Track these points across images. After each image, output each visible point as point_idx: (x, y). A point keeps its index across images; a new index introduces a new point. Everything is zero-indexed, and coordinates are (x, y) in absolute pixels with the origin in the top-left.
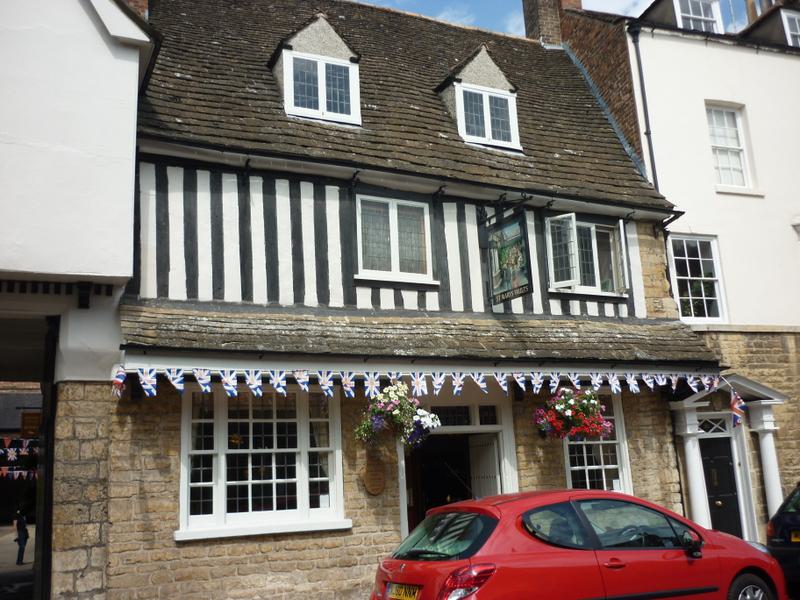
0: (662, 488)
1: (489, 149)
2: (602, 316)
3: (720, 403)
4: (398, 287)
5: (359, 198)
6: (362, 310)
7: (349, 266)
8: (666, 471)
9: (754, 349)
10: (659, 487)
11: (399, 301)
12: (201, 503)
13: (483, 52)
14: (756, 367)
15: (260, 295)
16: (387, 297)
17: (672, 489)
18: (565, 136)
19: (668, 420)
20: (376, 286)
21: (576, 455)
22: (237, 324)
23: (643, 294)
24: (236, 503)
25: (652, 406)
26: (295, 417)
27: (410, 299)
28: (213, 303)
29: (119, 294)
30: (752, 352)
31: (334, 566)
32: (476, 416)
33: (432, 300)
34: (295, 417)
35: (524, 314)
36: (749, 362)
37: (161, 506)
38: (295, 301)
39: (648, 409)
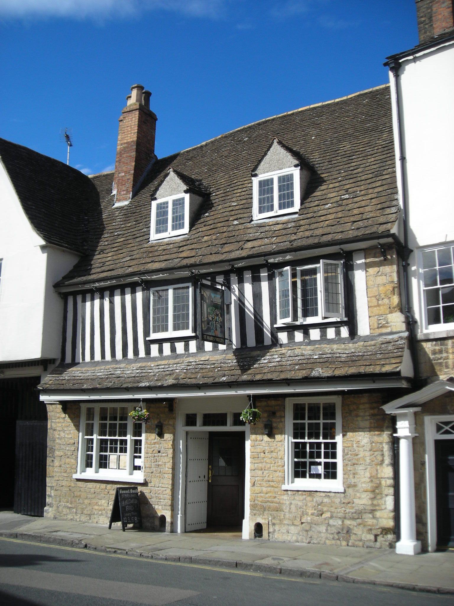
4: (172, 341)
6: (153, 358)
7: (146, 333)
10: (368, 480)
11: (173, 349)
18: (359, 179)
20: (160, 342)
21: (330, 450)
23: (367, 314)
25: (372, 411)
26: (127, 420)
27: (180, 347)
28: (185, 354)
32: (230, 420)
33: (345, 332)
34: (127, 420)
35: (288, 343)
37: (71, 462)
38: (123, 357)
39: (367, 414)
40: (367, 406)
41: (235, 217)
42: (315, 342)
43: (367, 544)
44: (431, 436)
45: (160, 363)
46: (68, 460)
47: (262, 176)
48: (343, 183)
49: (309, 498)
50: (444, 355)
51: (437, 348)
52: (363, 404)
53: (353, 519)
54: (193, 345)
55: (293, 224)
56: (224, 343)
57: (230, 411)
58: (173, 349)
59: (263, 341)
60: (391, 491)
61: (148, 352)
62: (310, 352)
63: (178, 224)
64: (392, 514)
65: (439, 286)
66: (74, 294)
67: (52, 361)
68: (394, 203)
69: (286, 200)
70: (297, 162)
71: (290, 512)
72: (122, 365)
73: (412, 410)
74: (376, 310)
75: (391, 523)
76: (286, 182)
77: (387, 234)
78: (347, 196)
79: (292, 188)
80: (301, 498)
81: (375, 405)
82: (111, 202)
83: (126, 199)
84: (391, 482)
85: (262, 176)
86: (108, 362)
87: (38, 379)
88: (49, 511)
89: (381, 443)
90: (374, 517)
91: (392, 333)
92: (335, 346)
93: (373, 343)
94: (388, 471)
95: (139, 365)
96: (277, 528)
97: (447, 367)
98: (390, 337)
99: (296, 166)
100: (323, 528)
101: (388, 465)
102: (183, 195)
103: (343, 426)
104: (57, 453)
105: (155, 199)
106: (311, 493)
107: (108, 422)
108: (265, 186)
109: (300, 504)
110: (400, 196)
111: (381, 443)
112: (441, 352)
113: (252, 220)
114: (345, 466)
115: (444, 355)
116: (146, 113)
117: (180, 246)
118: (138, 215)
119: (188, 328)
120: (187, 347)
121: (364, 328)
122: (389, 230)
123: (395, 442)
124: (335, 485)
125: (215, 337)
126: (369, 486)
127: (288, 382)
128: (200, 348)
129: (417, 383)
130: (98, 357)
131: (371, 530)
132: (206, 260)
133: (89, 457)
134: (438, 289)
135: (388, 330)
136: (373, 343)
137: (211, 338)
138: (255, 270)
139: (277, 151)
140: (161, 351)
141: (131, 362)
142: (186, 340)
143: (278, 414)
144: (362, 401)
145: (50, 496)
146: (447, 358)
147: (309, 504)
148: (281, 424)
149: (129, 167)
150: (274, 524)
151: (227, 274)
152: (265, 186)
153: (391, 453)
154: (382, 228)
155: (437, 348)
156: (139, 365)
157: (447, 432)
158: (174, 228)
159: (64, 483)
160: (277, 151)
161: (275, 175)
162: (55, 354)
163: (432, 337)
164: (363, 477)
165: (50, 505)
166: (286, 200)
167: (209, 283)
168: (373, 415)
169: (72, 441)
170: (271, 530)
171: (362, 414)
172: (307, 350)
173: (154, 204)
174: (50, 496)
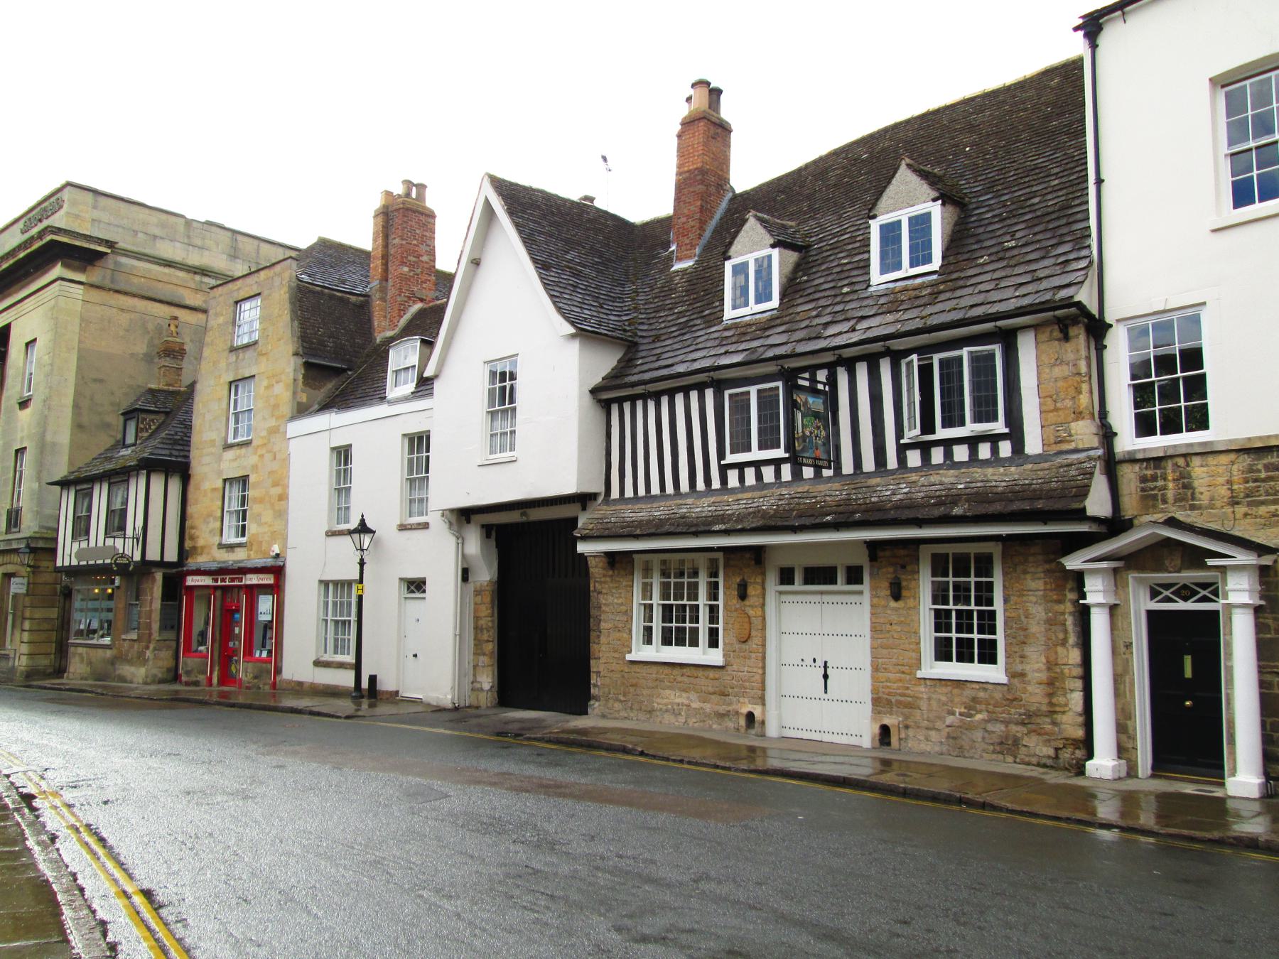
0: (1049, 669)
1: (899, 284)
2: (996, 459)
3: (1178, 562)
4: (757, 465)
5: (780, 384)
7: (721, 455)
8: (1060, 649)
9: (1263, 475)
11: (759, 476)
12: (648, 640)
13: (903, 167)
14: (1263, 503)
15: (670, 489)
16: (961, 453)
17: (1066, 671)
19: (1070, 585)
20: (741, 466)
22: (629, 514)
24: (666, 641)
25: (1047, 566)
29: (601, 499)
30: (1256, 480)
31: (714, 693)
32: (841, 577)
33: (1005, 449)
36: (1247, 496)
40: (1040, 557)
41: (846, 282)
42: (962, 464)
43: (1044, 761)
44: (1140, 604)
45: (740, 496)
46: (618, 635)
47: (884, 219)
48: (1009, 222)
49: (956, 691)
50: (1160, 483)
51: (1149, 472)
52: (1034, 554)
53: (1023, 724)
54: (786, 470)
55: (929, 290)
56: (829, 468)
57: (840, 562)
58: (759, 476)
59: (885, 464)
60: (1079, 684)
61: (724, 480)
62: (953, 480)
63: (763, 296)
64: (1081, 719)
65: (1153, 378)
66: (620, 401)
67: (593, 496)
68: (1084, 253)
69: (921, 253)
70: (936, 194)
71: (930, 710)
72: (690, 501)
73: (1104, 565)
74: (1052, 417)
75: (1080, 733)
76: (921, 224)
77: (1069, 303)
78: (1013, 243)
79: (910, 247)
80: (945, 690)
81: (1052, 557)
82: (669, 261)
83: (690, 257)
84: (1078, 671)
85: (884, 219)
86: (656, 496)
87: (574, 521)
88: (595, 706)
89: (1063, 614)
90: (1054, 723)
91: (1076, 451)
92: (990, 471)
93: (1046, 465)
94: (1075, 656)
95: (712, 499)
96: (911, 732)
97: (1165, 501)
98: (1075, 456)
99: (934, 200)
100: (978, 735)
101: (1073, 646)
102: (769, 251)
103: (1004, 586)
104: (603, 625)
105: (729, 258)
106: (960, 684)
107: (672, 580)
108: (891, 232)
109: (944, 698)
110: (1094, 242)
111: (1063, 614)
112: (1154, 478)
113: (869, 286)
114: (1008, 646)
115: (1160, 483)
116: (715, 124)
117: (765, 326)
118: (705, 287)
119: (778, 446)
120: (778, 474)
121: (1033, 445)
122: (1072, 297)
123: (1083, 614)
124: (994, 673)
125: (815, 459)
126: (1043, 676)
127: (919, 523)
128: (797, 474)
129: (1116, 525)
130: (655, 490)
131: (1049, 741)
132: (801, 348)
133: (648, 630)
134: (1153, 383)
135: (1072, 446)
136: (1046, 465)
137: (810, 461)
138: (873, 362)
139: (905, 179)
140: (742, 478)
141: (701, 495)
142: (777, 463)
143: (909, 568)
144: (1032, 551)
145: (595, 686)
146: (1165, 488)
147: (957, 700)
148: (913, 583)
149: (692, 208)
150: (907, 727)
151: (831, 367)
152: (891, 232)
153: (1078, 629)
154: (1063, 293)
155: (1149, 472)
156: (712, 499)
157: (1168, 600)
158: (758, 301)
159: (614, 666)
160: (905, 179)
161: (903, 216)
162: (598, 487)
163: (1140, 456)
164: (1035, 665)
165: (597, 699)
166: (921, 253)
167: (807, 384)
168: (1047, 572)
169: (623, 608)
170: (903, 736)
171: (1032, 570)
172: (948, 477)
173: (728, 266)
174: (595, 686)
